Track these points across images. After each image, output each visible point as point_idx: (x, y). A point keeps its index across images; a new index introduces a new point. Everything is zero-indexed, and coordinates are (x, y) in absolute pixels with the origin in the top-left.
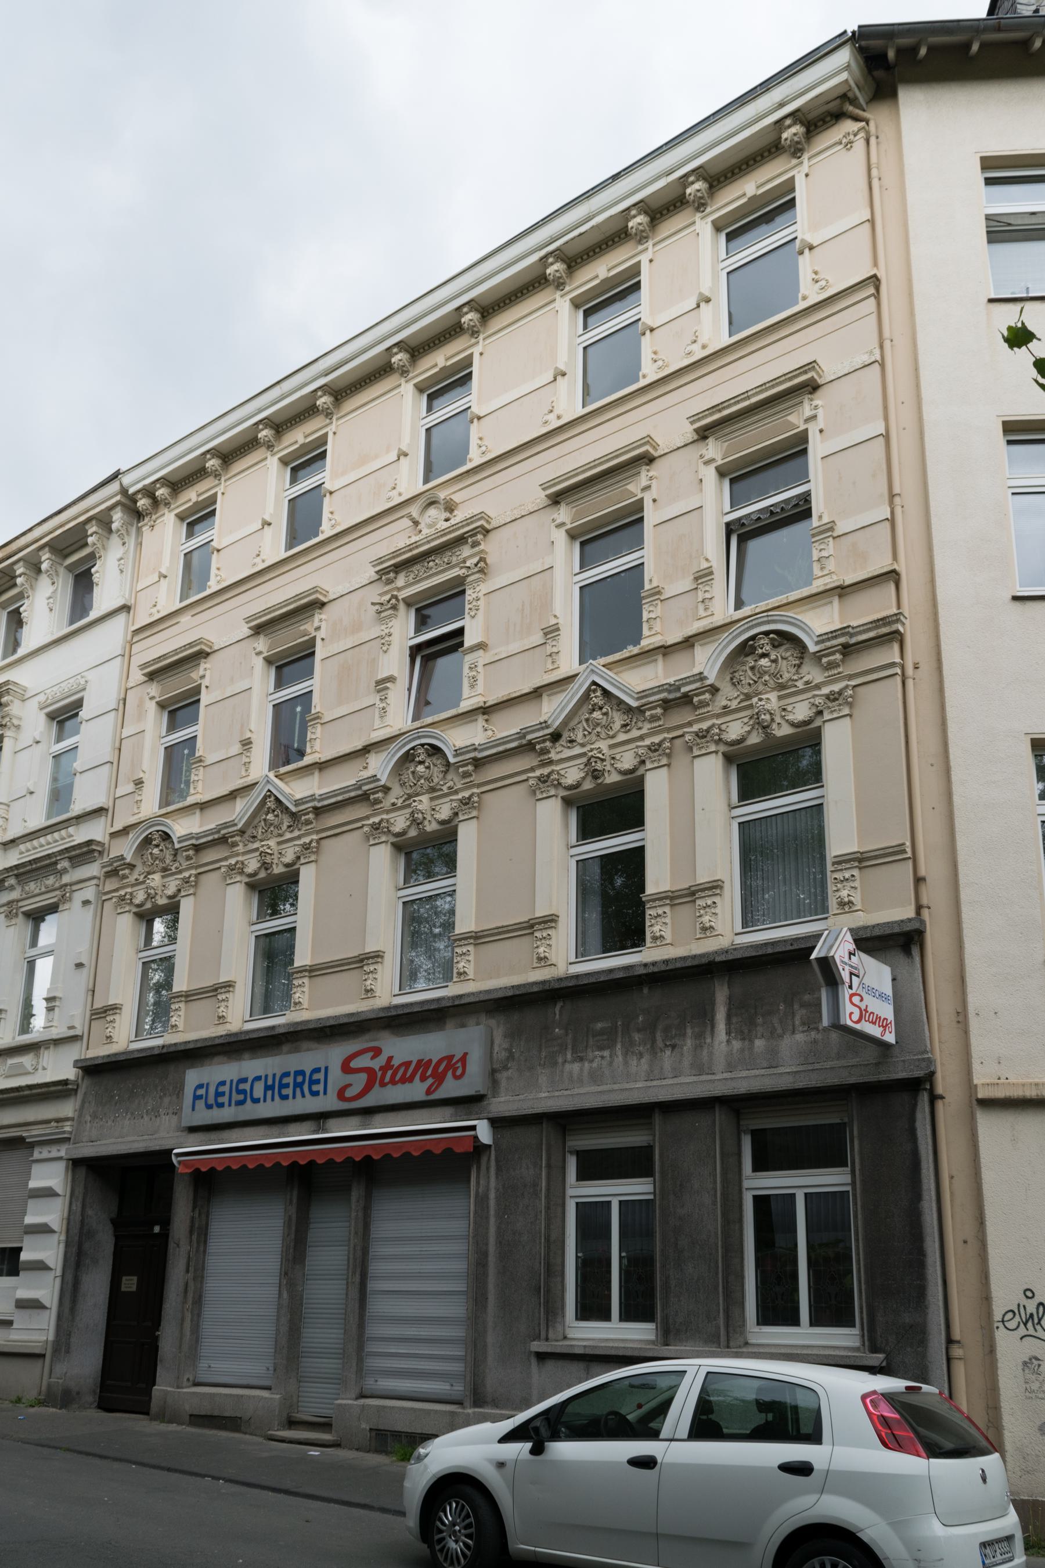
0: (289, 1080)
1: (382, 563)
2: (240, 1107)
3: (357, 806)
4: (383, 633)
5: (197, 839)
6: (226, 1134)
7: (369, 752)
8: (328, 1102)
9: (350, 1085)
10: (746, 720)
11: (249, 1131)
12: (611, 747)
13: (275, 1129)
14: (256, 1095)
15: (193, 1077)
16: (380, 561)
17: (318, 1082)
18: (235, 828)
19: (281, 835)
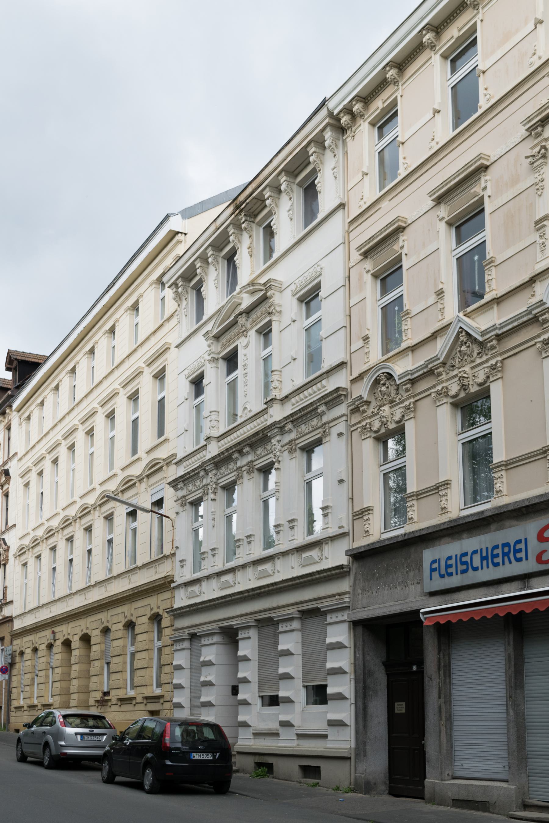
0: (499, 551)
1: (530, 121)
2: (464, 575)
3: (529, 328)
4: (537, 180)
5: (412, 374)
6: (456, 596)
7: (535, 282)
8: (530, 565)
9: (545, 551)
11: (472, 592)
12: (472, 368)
13: (492, 590)
14: (475, 565)
15: (428, 555)
16: (529, 119)
17: (520, 550)
18: (438, 362)
19: (473, 362)
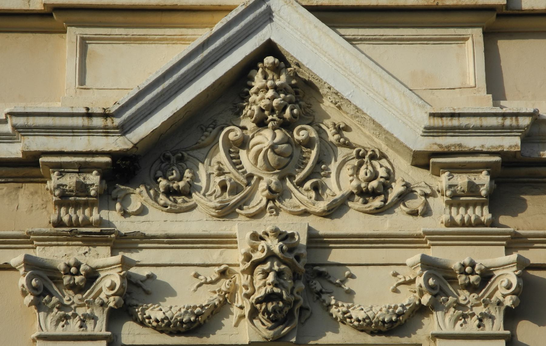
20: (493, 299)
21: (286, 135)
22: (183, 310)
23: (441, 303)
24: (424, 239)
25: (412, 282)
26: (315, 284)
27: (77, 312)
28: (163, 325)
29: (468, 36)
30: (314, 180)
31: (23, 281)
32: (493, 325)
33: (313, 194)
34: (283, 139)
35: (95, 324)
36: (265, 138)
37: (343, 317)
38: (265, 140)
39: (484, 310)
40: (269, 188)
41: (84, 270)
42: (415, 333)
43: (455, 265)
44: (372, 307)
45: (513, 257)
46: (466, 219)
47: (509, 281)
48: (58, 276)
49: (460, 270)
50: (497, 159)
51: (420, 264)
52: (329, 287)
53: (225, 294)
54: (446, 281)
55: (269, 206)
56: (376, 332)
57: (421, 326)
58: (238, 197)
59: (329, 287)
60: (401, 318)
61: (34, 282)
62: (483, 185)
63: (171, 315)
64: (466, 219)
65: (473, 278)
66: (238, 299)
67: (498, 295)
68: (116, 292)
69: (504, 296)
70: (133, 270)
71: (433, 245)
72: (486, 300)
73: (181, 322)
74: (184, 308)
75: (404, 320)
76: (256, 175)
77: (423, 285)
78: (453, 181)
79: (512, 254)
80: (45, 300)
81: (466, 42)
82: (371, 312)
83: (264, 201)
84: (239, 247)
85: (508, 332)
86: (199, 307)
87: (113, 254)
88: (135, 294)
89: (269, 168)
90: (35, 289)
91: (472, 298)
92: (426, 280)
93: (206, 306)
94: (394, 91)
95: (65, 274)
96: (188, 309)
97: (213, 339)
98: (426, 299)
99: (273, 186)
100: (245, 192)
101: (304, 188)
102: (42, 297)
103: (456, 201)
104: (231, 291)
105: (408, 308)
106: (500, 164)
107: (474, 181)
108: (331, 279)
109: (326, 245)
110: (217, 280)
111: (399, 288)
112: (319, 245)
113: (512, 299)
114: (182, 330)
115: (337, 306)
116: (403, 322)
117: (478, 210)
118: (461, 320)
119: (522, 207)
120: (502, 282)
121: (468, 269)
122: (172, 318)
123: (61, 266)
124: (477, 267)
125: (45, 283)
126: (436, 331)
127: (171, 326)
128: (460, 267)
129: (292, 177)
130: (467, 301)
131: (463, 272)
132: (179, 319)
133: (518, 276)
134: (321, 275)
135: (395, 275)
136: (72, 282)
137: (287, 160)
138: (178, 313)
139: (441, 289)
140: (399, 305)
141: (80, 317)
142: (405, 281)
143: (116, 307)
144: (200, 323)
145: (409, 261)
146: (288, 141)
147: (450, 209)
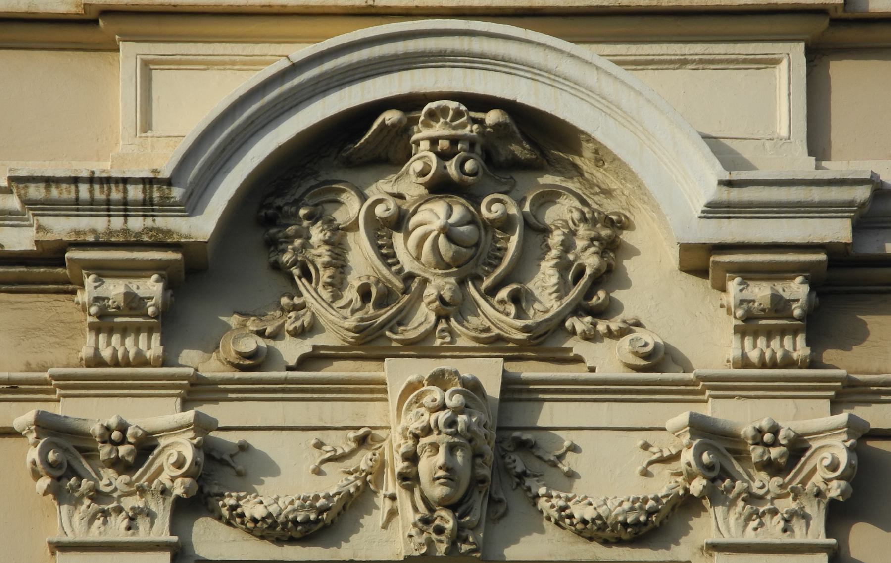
10: (342, 442)
20: (809, 486)
21: (467, 208)
22: (297, 503)
23: (722, 492)
24: (699, 387)
25: (676, 457)
26: (515, 461)
27: (122, 505)
28: (265, 526)
29: (780, 56)
30: (515, 286)
31: (33, 454)
32: (152, 526)
33: (512, 309)
34: (462, 218)
35: (152, 524)
36: (434, 215)
37: (561, 516)
38: (435, 219)
39: (794, 506)
40: (441, 298)
41: (134, 435)
42: (347, 541)
43: (747, 431)
44: (277, 499)
45: (842, 417)
46: (768, 356)
47: (179, 453)
48: (89, 445)
49: (754, 438)
50: (822, 257)
51: (688, 428)
52: (535, 466)
53: (366, 476)
54: (77, 453)
55: (440, 327)
56: (614, 540)
57: (687, 530)
58: (386, 314)
59: (535, 466)
60: (325, 515)
61: (706, 457)
62: (797, 300)
63: (607, 513)
64: (768, 356)
65: (774, 452)
66: (387, 486)
67: (816, 481)
68: (842, 473)
69: (173, 479)
70: (213, 434)
71: (65, 396)
72: (797, 488)
73: (295, 522)
74: (299, 499)
75: (659, 520)
76: (419, 276)
77: (693, 463)
78: (747, 294)
79: (841, 412)
80: (70, 485)
81: (778, 67)
82: (605, 507)
83: (432, 318)
84: (389, 399)
85: (833, 541)
86: (653, 499)
87: (833, 412)
88: (217, 472)
89: (440, 263)
90: (709, 467)
91: (121, 481)
92: (698, 456)
93: (334, 495)
94: (682, 140)
95: (104, 442)
96: (633, 502)
97: (345, 551)
98: (697, 486)
99: (447, 296)
100: (401, 304)
101: (497, 298)
102: (65, 480)
103: (753, 325)
104: (374, 470)
105: (664, 501)
106: (826, 264)
107: (136, 291)
108: (539, 453)
109: (534, 396)
110: (352, 453)
111: (324, 467)
112: (516, 396)
113: (839, 487)
114: (297, 535)
115: (550, 497)
116: (658, 524)
117: (788, 341)
118: (99, 519)
119: (859, 335)
120: (170, 455)
121: (116, 435)
122: (607, 518)
123: (95, 429)
124: (130, 431)
125: (68, 457)
126: (715, 538)
127: (278, 529)
128: (102, 431)
129: (477, 279)
130: (765, 490)
131: (758, 440)
132: (290, 516)
133: (850, 449)
134: (524, 446)
135: (646, 447)
136: (113, 456)
137: (471, 252)
138: (290, 508)
139: (70, 466)
140: (321, 495)
141: (127, 513)
142: (662, 456)
143: (841, 499)
144: (322, 525)
145: (670, 424)
146: (473, 220)
147: (97, 335)
